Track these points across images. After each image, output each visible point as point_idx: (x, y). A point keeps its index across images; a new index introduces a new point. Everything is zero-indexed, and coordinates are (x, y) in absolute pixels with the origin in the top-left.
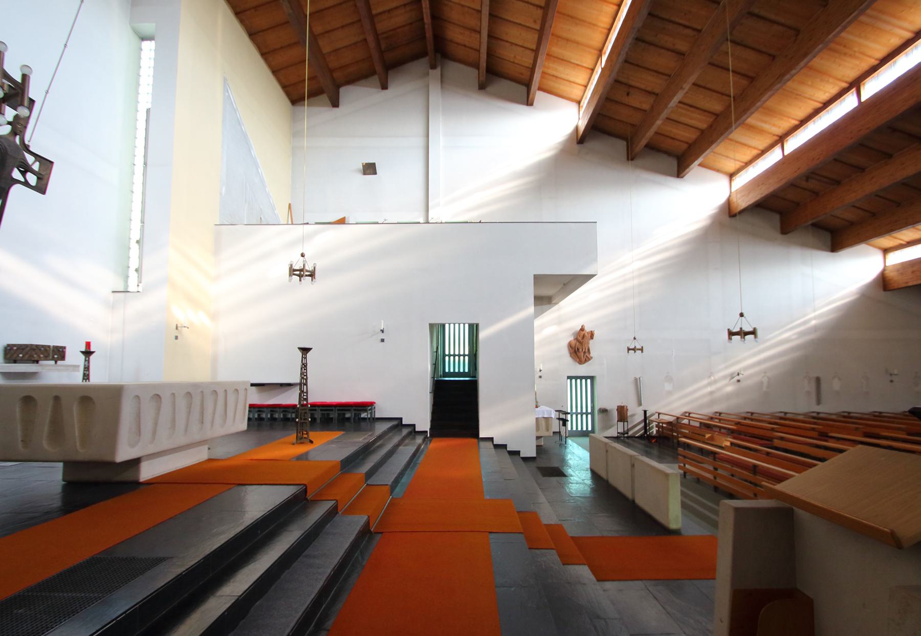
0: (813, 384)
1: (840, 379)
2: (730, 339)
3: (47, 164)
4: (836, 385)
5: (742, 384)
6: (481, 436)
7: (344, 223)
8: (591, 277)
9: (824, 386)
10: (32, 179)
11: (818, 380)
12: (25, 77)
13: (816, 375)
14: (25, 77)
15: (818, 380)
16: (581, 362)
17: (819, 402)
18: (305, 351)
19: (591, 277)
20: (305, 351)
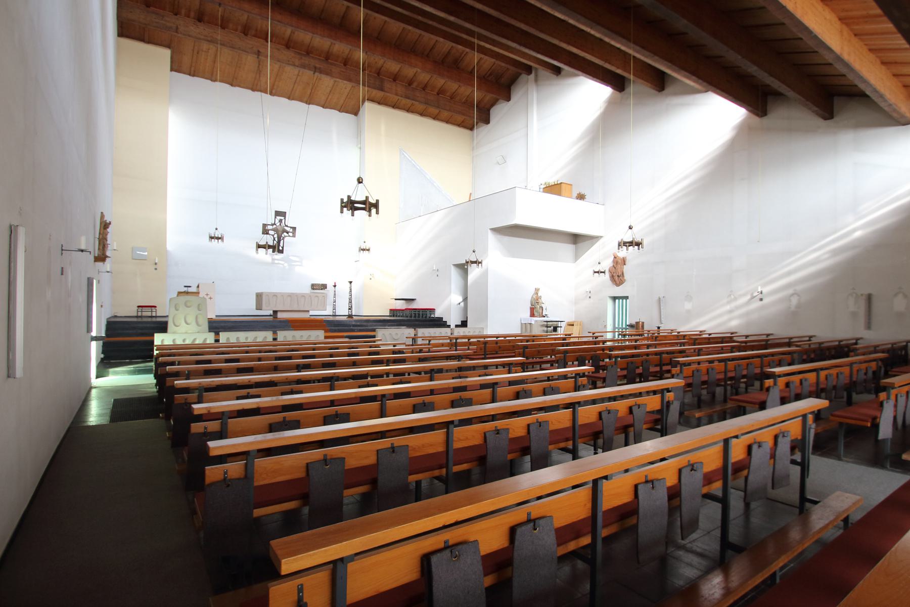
0: (862, 304)
1: (905, 296)
2: (377, 201)
3: (294, 229)
4: (900, 304)
5: (765, 301)
6: (283, 573)
7: (559, 193)
8: (607, 212)
9: (877, 306)
10: (291, 234)
11: (869, 298)
12: (342, 212)
13: (866, 292)
14: (342, 212)
15: (869, 298)
16: (618, 285)
17: (869, 326)
18: (351, 282)
19: (607, 212)
20: (351, 282)
